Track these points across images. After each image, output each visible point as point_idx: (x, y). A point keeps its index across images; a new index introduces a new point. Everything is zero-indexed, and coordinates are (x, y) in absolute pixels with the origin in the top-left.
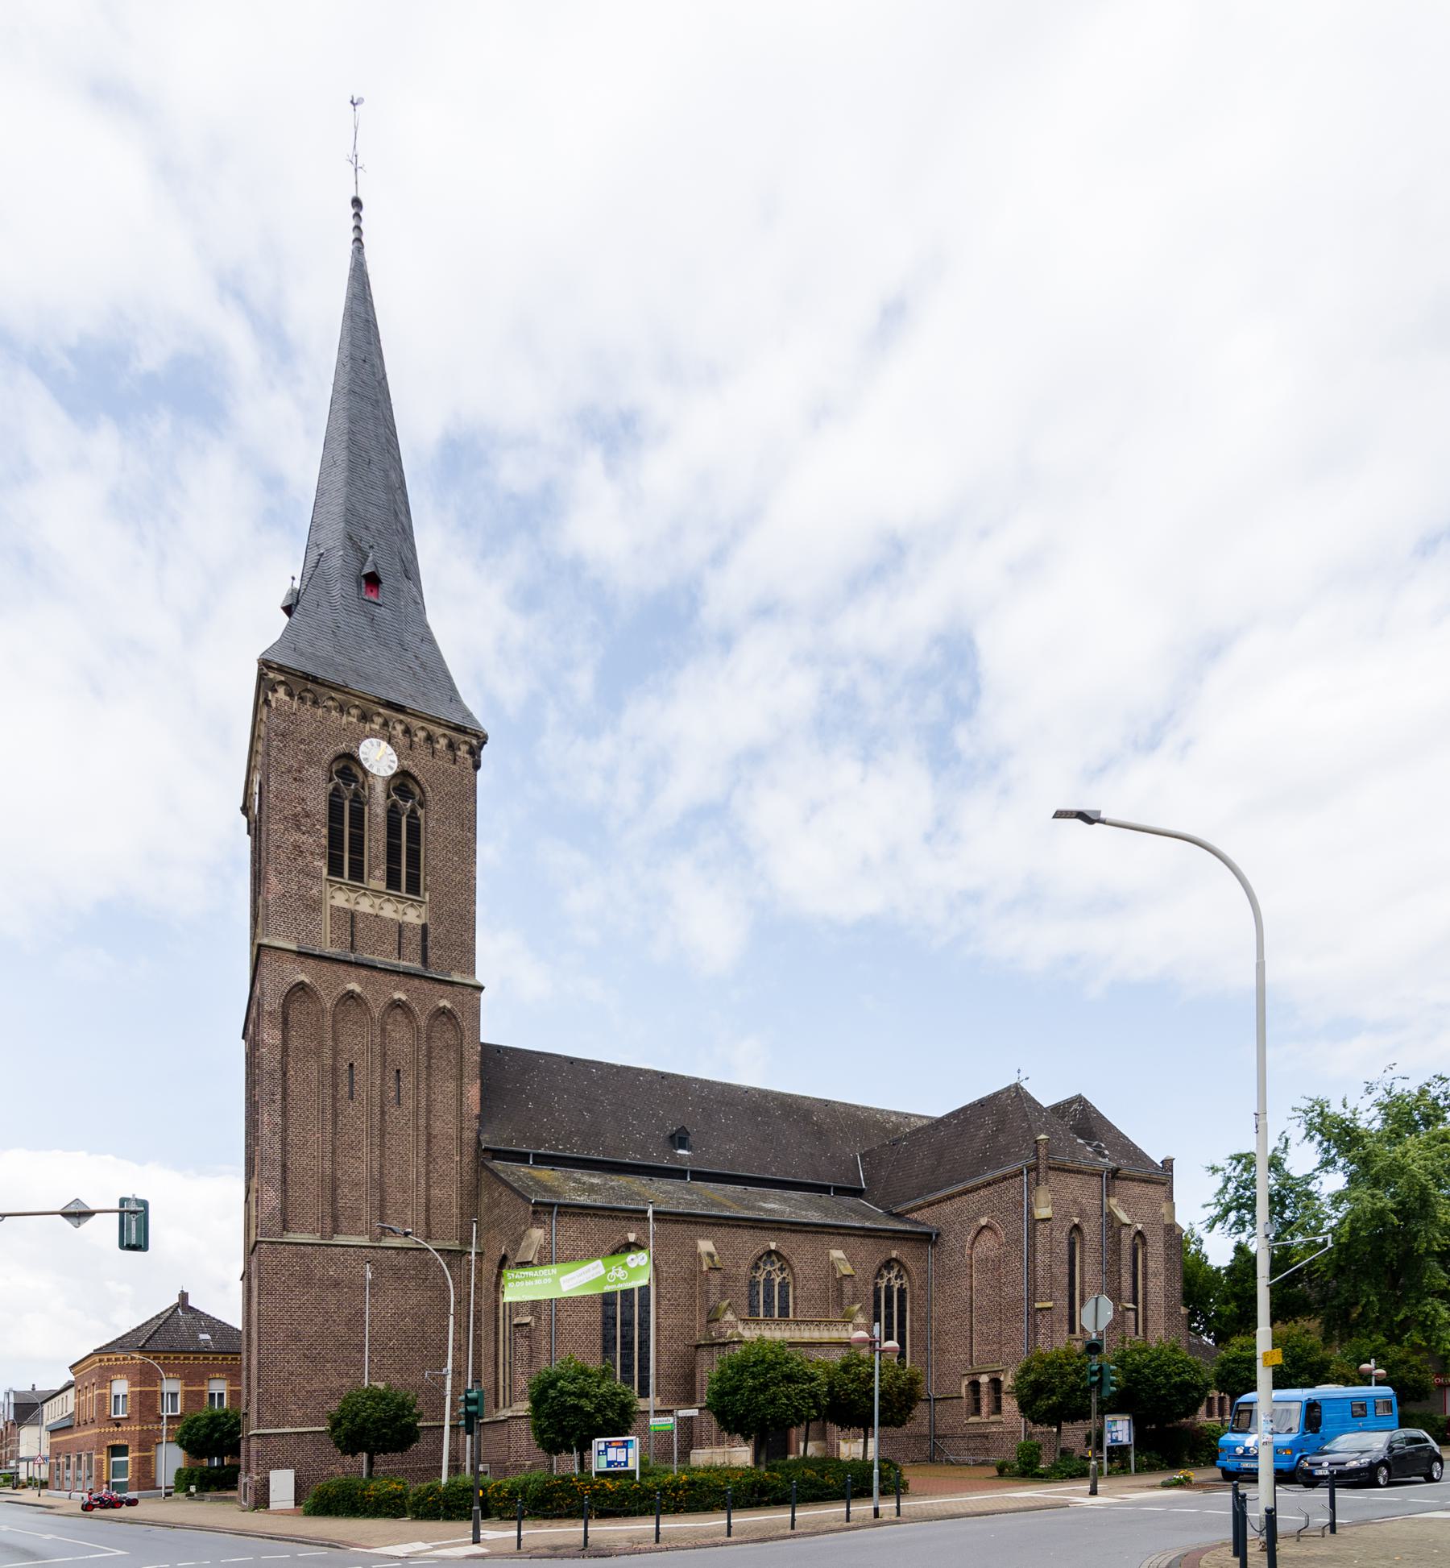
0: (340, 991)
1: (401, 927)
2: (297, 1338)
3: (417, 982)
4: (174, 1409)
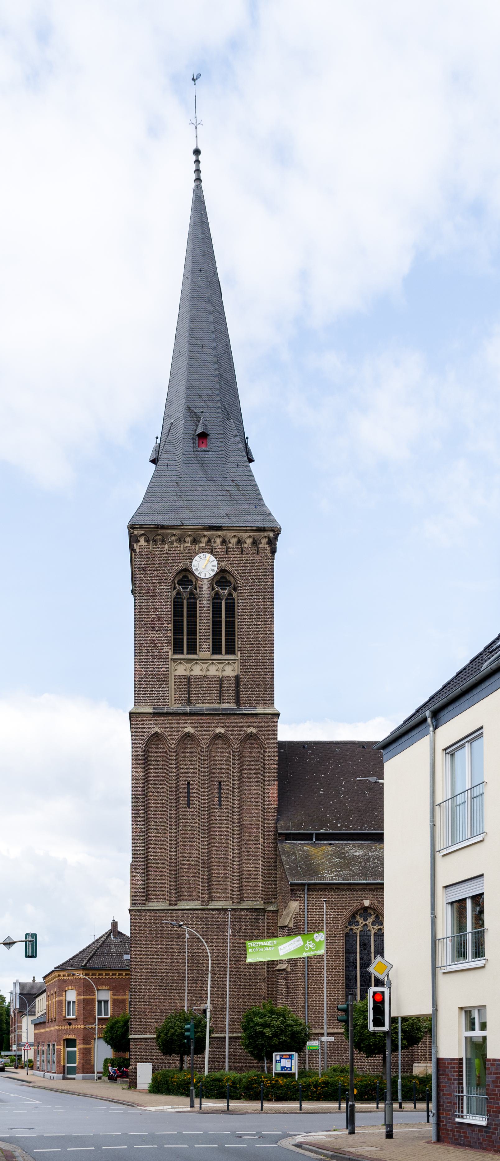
0: (181, 734)
1: (221, 681)
2: (153, 973)
3: (231, 718)
4: (106, 1013)
